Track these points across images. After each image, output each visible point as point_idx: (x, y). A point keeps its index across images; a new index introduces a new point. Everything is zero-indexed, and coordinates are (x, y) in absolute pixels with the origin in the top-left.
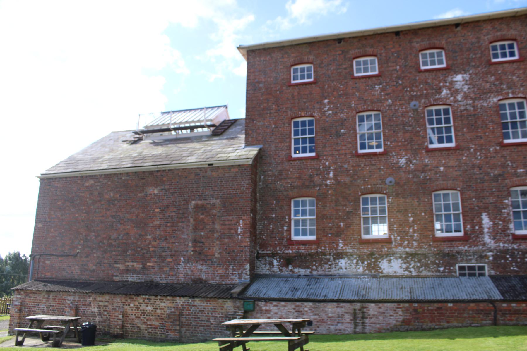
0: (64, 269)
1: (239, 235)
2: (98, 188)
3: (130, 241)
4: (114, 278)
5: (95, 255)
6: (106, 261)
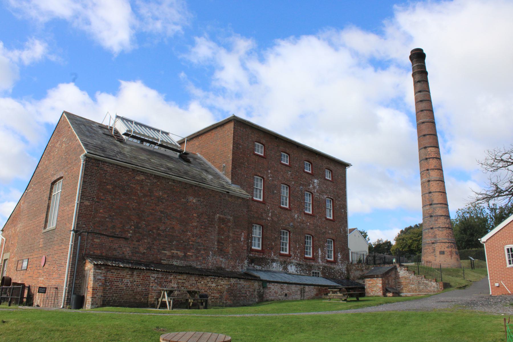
0: (115, 249)
1: (242, 242)
2: (149, 184)
3: (175, 234)
4: (162, 261)
5: (146, 241)
6: (155, 247)
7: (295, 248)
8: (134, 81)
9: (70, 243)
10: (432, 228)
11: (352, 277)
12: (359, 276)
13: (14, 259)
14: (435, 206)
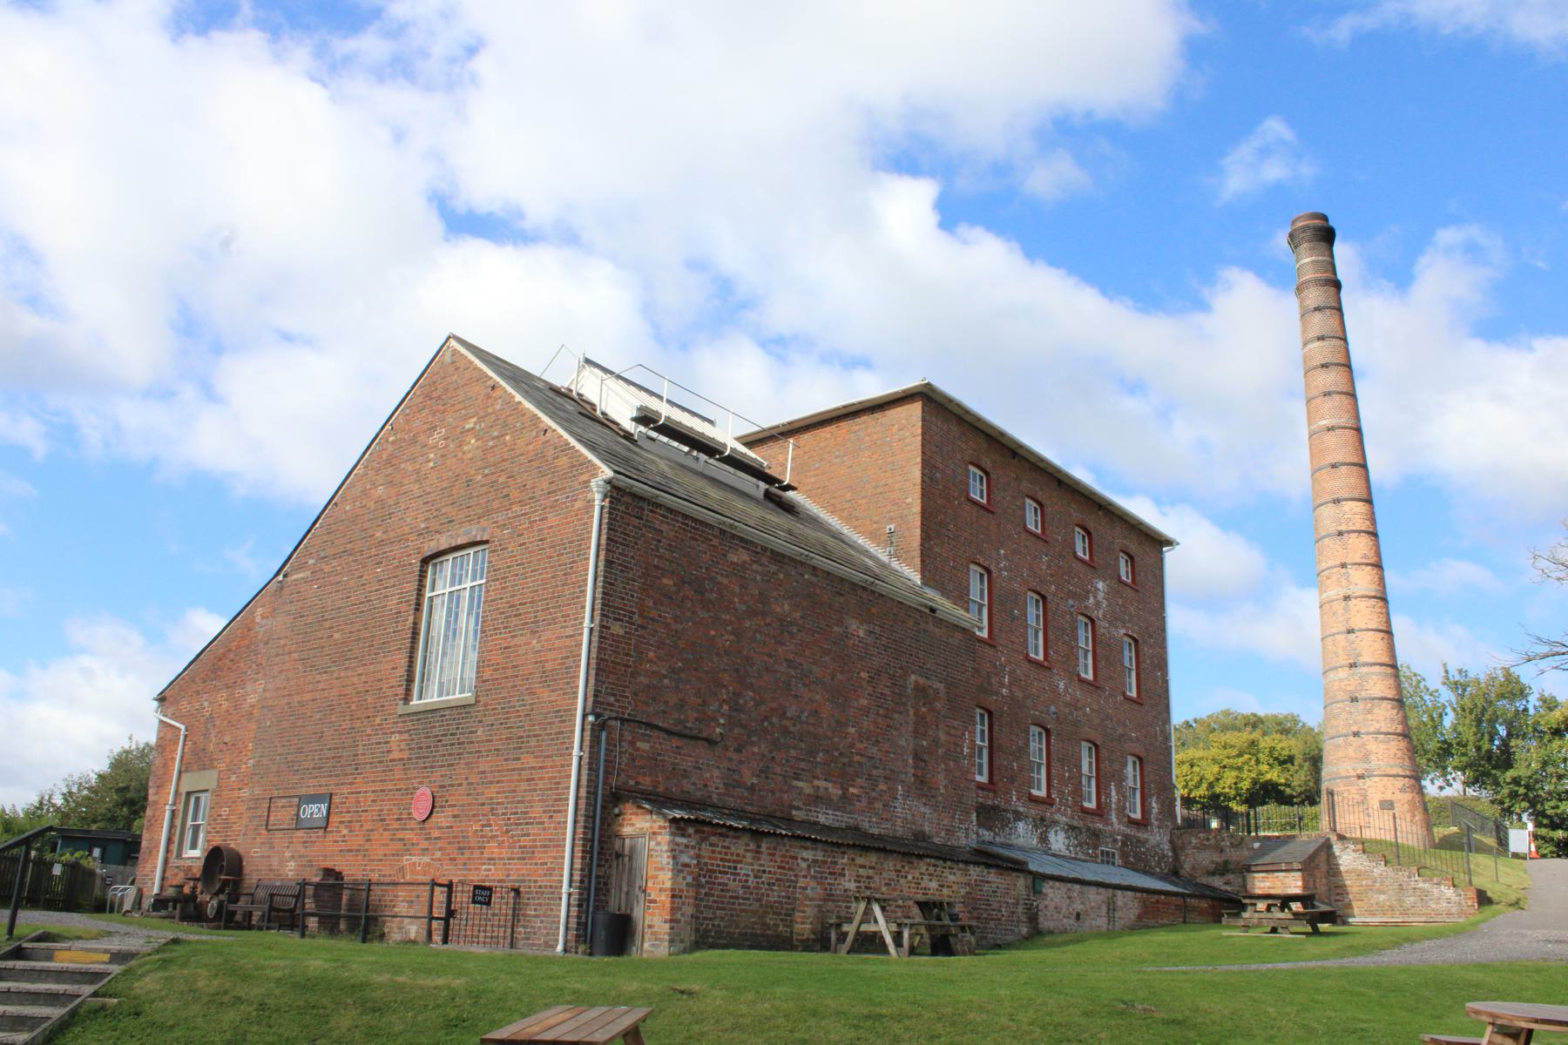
3: (820, 731)
6: (778, 769)
7: (1061, 779)
8: (1104, 292)
9: (576, 751)
10: (1356, 734)
11: (1187, 866)
12: (1212, 867)
13: (245, 793)
14: (1365, 669)
